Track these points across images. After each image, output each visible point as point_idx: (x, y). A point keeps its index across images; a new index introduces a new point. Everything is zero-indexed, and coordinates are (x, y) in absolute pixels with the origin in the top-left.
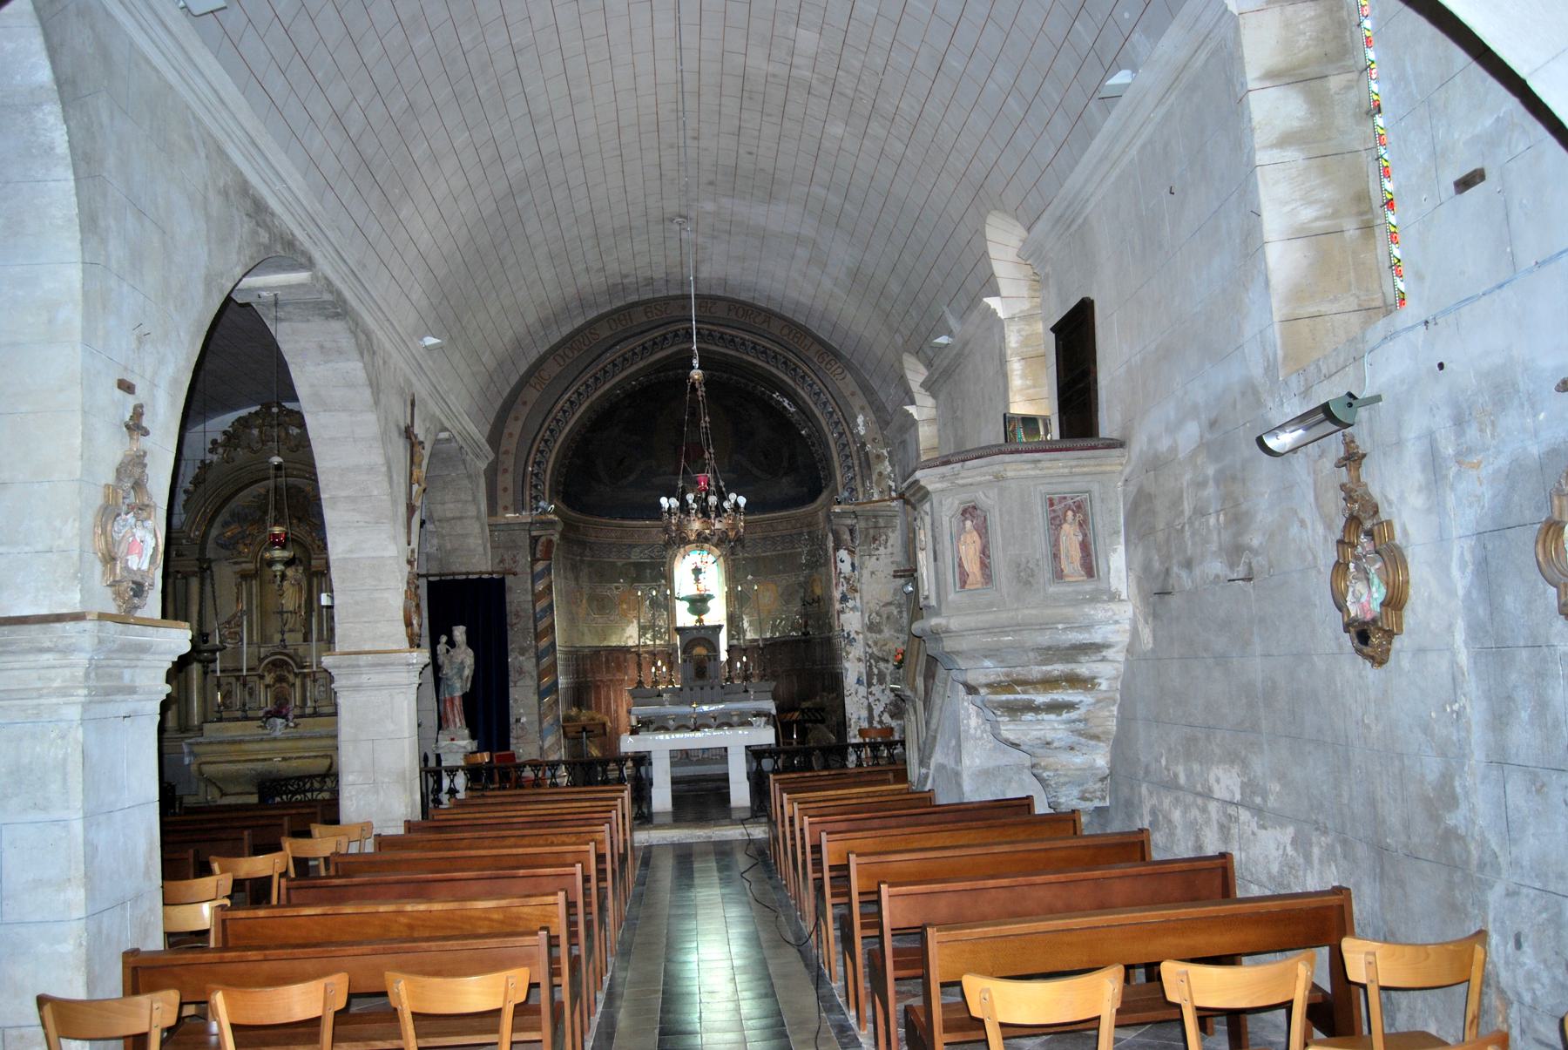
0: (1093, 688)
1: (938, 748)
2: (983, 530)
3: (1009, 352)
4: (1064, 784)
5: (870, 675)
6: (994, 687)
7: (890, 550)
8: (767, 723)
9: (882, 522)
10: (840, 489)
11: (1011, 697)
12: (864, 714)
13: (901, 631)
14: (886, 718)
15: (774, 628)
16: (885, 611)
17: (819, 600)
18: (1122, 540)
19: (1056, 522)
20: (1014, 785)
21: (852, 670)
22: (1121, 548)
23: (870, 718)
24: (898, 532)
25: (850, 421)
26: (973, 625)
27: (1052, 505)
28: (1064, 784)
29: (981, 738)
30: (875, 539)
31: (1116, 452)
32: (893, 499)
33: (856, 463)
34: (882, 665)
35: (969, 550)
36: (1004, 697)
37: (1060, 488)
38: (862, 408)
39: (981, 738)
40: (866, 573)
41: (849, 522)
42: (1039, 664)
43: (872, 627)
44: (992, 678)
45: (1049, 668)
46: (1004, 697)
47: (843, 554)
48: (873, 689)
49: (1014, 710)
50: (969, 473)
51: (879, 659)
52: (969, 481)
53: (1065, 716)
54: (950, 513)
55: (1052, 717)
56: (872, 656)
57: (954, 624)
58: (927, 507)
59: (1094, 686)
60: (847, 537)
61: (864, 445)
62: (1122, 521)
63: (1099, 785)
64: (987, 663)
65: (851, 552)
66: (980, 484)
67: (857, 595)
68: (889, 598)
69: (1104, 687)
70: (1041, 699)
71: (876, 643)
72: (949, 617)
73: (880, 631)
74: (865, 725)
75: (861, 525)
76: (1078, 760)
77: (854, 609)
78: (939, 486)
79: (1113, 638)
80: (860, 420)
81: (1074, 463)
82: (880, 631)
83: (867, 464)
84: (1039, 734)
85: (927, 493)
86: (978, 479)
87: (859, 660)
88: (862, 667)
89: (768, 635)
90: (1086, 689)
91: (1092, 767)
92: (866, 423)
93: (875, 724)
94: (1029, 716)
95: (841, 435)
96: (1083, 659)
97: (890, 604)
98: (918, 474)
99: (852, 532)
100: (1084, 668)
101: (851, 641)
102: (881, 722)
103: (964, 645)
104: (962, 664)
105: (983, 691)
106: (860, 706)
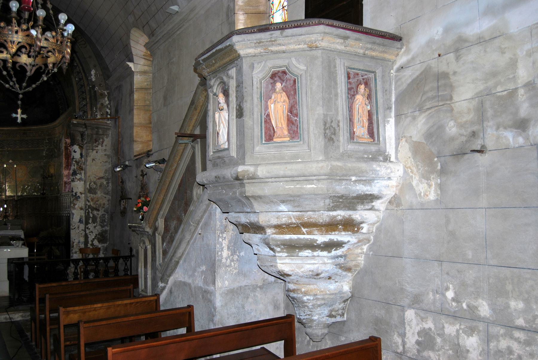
0: (357, 231)
1: (178, 270)
2: (292, 91)
3: (237, 8)
4: (319, 306)
5: (87, 218)
6: (280, 228)
7: (104, 148)
8: (23, 244)
9: (101, 132)
10: (77, 110)
11: (295, 237)
12: (82, 239)
13: (107, 194)
14: (96, 243)
15: (24, 190)
16: (99, 182)
17: (52, 176)
18: (393, 114)
19: (352, 93)
20: (250, 300)
21: (77, 215)
22: (392, 121)
23: (86, 242)
24: (109, 139)
25: (87, 74)
26: (282, 173)
27: (349, 78)
28: (319, 306)
29: (230, 266)
30: (96, 141)
31: (398, 44)
32: (108, 119)
33: (88, 97)
34: (95, 212)
35: (278, 108)
36: (287, 237)
37: (356, 66)
38: (95, 66)
39: (230, 266)
40: (89, 159)
41: (81, 129)
42: (329, 210)
43: (91, 191)
44: (284, 220)
45: (334, 213)
46: (287, 237)
47: (76, 148)
48: (89, 226)
49: (292, 247)
50: (286, 41)
51: (93, 209)
52: (283, 48)
53: (334, 253)
54: (261, 76)
55: (325, 253)
56: (90, 207)
57: (261, 171)
58: (233, 72)
59: (359, 229)
60: (79, 138)
61: (94, 87)
62: (393, 100)
63: (342, 305)
64: (283, 207)
65: (81, 147)
66: (293, 51)
67: (83, 172)
68: (102, 175)
69: (364, 231)
70: (321, 238)
71: (92, 200)
72: (257, 165)
73: (95, 193)
74: (82, 246)
75: (88, 132)
76: (332, 287)
77: (80, 179)
78: (251, 51)
79: (385, 192)
80: (93, 72)
81: (369, 46)
82: (95, 193)
83: (94, 98)
84: (312, 267)
85: (239, 57)
86: (292, 47)
87: (81, 209)
88: (82, 213)
89: (19, 194)
90: (354, 232)
91: (341, 292)
92: (96, 75)
93: (89, 246)
94: (307, 253)
95: (80, 79)
96: (360, 207)
97: (102, 178)
98: (235, 39)
99: (82, 135)
100: (356, 215)
101: (77, 198)
102: (92, 245)
103: (267, 190)
104: (257, 206)
105: (269, 231)
106: (82, 234)
